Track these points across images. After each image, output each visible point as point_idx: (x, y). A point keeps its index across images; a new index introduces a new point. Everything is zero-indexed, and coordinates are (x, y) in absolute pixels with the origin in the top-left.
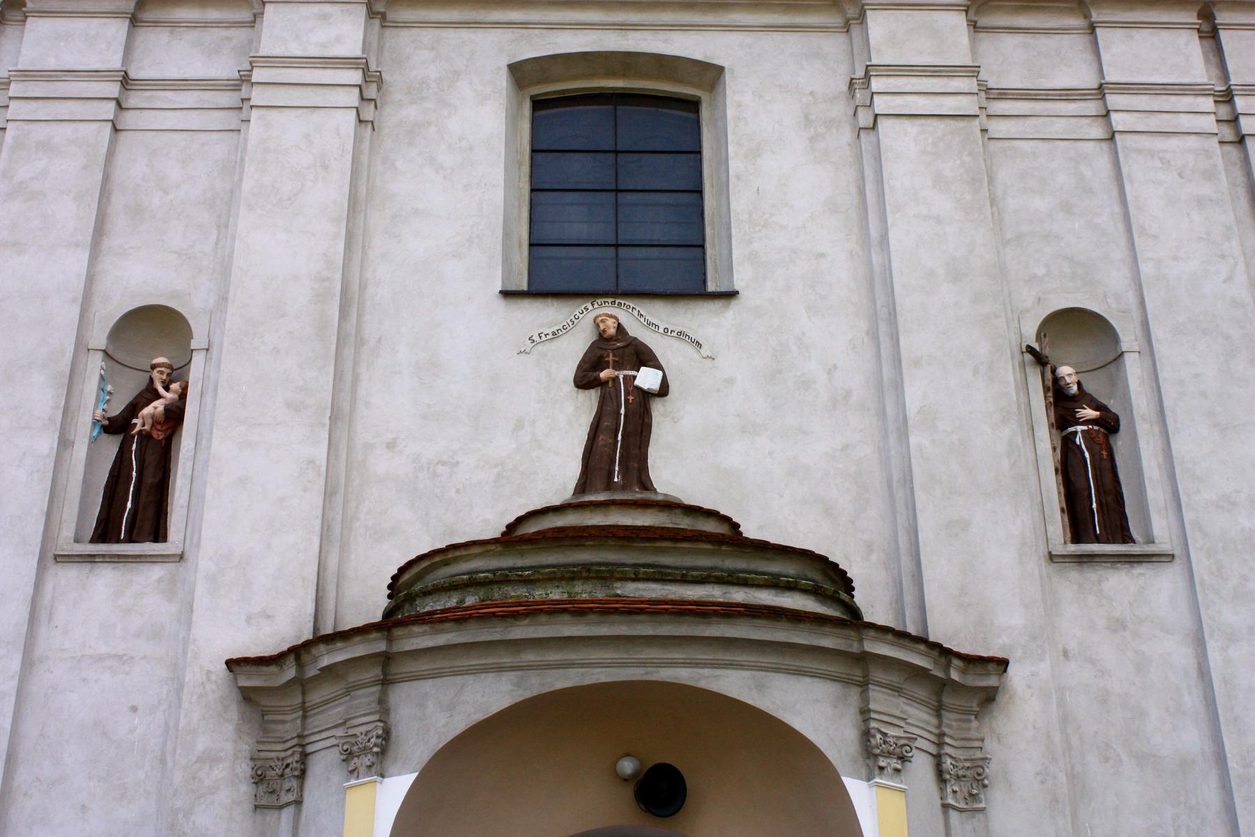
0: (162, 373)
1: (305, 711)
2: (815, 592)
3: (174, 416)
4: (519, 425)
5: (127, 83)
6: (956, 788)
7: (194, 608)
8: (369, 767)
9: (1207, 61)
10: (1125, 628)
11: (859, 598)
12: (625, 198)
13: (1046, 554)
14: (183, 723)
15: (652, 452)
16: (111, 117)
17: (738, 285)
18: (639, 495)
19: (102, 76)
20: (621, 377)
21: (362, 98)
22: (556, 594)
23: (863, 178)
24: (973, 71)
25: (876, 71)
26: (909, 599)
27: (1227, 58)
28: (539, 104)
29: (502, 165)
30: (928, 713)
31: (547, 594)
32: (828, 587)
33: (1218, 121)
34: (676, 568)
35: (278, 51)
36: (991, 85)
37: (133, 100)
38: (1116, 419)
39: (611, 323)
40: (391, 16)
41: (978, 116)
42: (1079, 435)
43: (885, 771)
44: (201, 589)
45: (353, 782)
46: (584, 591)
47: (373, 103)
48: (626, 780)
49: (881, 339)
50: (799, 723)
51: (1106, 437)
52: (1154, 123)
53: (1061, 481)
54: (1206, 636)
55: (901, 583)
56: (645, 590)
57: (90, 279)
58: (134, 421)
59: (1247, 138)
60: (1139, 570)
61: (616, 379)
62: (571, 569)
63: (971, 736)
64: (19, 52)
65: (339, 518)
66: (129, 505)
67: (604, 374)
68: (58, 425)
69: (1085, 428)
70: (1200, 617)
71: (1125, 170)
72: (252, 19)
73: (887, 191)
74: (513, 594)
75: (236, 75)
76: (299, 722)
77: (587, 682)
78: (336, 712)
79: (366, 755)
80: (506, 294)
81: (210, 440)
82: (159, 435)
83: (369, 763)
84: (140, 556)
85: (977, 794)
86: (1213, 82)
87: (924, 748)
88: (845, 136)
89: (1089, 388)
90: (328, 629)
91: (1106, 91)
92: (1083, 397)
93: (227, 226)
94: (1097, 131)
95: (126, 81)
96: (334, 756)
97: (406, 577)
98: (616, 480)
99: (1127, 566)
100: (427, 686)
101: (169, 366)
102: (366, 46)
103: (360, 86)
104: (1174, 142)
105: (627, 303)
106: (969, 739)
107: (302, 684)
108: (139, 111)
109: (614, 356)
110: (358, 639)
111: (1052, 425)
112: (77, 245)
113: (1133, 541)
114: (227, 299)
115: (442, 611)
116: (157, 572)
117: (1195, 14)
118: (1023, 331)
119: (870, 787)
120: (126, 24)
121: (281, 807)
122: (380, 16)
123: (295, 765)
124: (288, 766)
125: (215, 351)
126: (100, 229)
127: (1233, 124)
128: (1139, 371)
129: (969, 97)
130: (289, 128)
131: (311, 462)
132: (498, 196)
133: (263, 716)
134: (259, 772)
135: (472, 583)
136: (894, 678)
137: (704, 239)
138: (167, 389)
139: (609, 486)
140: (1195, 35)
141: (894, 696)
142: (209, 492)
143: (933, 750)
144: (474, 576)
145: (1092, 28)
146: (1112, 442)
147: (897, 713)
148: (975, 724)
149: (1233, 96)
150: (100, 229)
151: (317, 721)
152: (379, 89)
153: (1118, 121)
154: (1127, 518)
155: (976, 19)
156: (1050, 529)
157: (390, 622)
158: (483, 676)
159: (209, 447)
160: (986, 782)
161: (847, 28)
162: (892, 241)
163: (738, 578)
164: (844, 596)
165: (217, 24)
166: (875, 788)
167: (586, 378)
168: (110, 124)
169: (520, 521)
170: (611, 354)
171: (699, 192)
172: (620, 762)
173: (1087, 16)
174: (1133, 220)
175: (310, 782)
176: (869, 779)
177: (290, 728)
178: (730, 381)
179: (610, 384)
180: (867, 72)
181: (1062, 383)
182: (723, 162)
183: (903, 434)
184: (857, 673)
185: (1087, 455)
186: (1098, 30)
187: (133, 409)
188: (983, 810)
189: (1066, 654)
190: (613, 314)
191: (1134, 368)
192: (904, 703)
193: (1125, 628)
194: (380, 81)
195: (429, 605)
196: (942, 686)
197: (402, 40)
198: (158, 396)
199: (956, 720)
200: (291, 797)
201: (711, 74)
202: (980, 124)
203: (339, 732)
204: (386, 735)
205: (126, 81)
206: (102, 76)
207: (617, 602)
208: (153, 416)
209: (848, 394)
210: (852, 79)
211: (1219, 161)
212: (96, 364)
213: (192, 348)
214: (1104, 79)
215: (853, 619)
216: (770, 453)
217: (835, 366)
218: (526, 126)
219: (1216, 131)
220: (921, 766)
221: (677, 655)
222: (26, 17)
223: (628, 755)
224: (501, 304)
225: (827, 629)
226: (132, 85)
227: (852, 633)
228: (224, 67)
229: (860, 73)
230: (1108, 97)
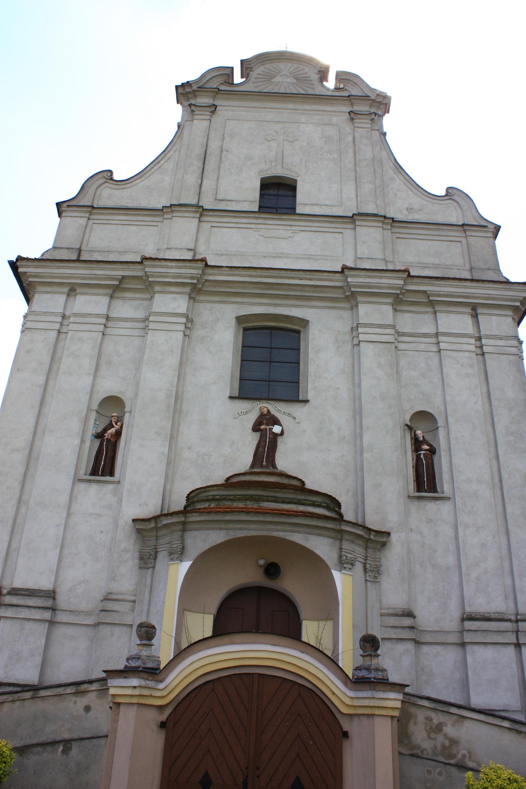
0: (115, 419)
1: (157, 538)
2: (327, 508)
3: (118, 434)
4: (233, 443)
5: (108, 319)
6: (370, 574)
7: (123, 501)
8: (177, 558)
9: (473, 325)
10: (432, 522)
11: (343, 510)
12: (272, 364)
13: (407, 495)
14: (117, 538)
15: (277, 455)
16: (102, 330)
17: (309, 398)
18: (271, 470)
19: (100, 316)
20: (268, 428)
21: (186, 327)
22: (241, 505)
23: (354, 362)
24: (393, 327)
25: (360, 325)
26: (360, 509)
27: (480, 325)
28: (245, 329)
29: (232, 352)
30: (362, 549)
31: (238, 505)
32: (332, 506)
33: (476, 347)
34: (281, 498)
35: (158, 310)
36: (400, 331)
37: (110, 324)
38: (435, 450)
39: (265, 410)
40: (197, 298)
41: (394, 343)
42: (422, 455)
43: (346, 569)
44: (125, 494)
45: (172, 562)
46: (250, 504)
47: (189, 329)
48: (261, 566)
49: (357, 419)
50: (318, 552)
51: (431, 455)
52: (454, 347)
53: (415, 471)
54: (459, 526)
55: (358, 504)
56: (270, 505)
57: (93, 386)
58: (105, 434)
59: (485, 354)
60: (438, 502)
61: (266, 429)
62: (246, 497)
63: (377, 557)
64: (74, 306)
65: (171, 472)
66: (102, 463)
67: (262, 427)
68: (81, 435)
69: (424, 452)
70: (457, 519)
71: (443, 363)
72: (150, 297)
73: (361, 367)
74: (227, 504)
75: (144, 317)
76: (155, 541)
77: (249, 535)
78: (167, 539)
79: (176, 554)
80: (231, 398)
81: (130, 443)
82: (113, 440)
83: (177, 557)
84: (106, 481)
85: (377, 577)
86: (475, 333)
87: (360, 561)
88: (349, 347)
89: (426, 438)
90: (165, 512)
91: (439, 335)
92: (425, 441)
93: (139, 369)
94: (435, 349)
95: (108, 318)
96: (165, 553)
97: (192, 495)
98: (264, 464)
99: (434, 501)
100: (197, 533)
101: (118, 417)
102: (188, 310)
103: (185, 324)
104: (461, 354)
105: (271, 403)
106: (376, 558)
107: (156, 529)
108: (111, 328)
109: (266, 421)
110: (175, 516)
111: (413, 451)
112: (89, 374)
113: (437, 492)
114: (137, 395)
115: (204, 509)
116: (111, 487)
117: (470, 309)
118: (405, 418)
119: (341, 573)
120: (109, 298)
121: (148, 568)
122: (193, 299)
123: (153, 555)
124: (151, 555)
125: (133, 412)
126: (97, 369)
127: (481, 348)
128: (443, 433)
129: (391, 336)
130: (161, 337)
131: (163, 453)
132: (230, 363)
133: (143, 538)
134: (142, 557)
135: (214, 500)
136: (351, 538)
137: (299, 380)
138: (116, 424)
139: (262, 466)
140: (470, 316)
141: (351, 544)
142: (129, 461)
143: (363, 561)
144: (214, 497)
145: (435, 312)
146: (433, 458)
147: (352, 549)
148: (378, 553)
149: (481, 339)
150: (97, 369)
151: (161, 541)
152: (192, 324)
153: (442, 346)
154: (436, 484)
155: (396, 307)
156: (410, 487)
157: (185, 512)
158: (215, 531)
159: (130, 446)
160: (380, 573)
161: (352, 308)
162: (362, 385)
163: (301, 502)
164: (337, 509)
165: (138, 299)
166: (342, 574)
167: (256, 428)
168: (102, 333)
169: (231, 477)
170: (265, 420)
171: (298, 363)
172: (260, 560)
173: (434, 308)
174: (445, 381)
175: (158, 561)
176: (340, 571)
177: (152, 543)
178: (305, 431)
179: (264, 430)
180: (357, 325)
181: (417, 436)
182: (307, 354)
183: (362, 453)
184: (339, 536)
185: (424, 462)
186: (437, 314)
187: (105, 430)
188: (379, 582)
189: (411, 530)
190: (267, 406)
191: (442, 432)
192: (354, 546)
193: (432, 522)
194: (192, 321)
195: (199, 506)
196: (368, 540)
197: (200, 307)
198: (113, 427)
199: (372, 552)
200: (152, 565)
201: (305, 323)
202: (395, 345)
203: (168, 545)
204: (183, 548)
205: (108, 318)
206: (100, 316)
207: (260, 509)
208: (111, 433)
209: (345, 437)
210: (352, 327)
211: (475, 361)
212: (94, 415)
213: (125, 411)
214: (438, 331)
215: (340, 518)
216: (317, 457)
217: (341, 427)
218: (241, 338)
219: (475, 351)
220: (359, 567)
221: (279, 527)
222: (77, 295)
223: (262, 558)
224: (228, 401)
225: (330, 521)
226: (110, 319)
227: (338, 523)
228: (140, 314)
229: (355, 325)
230: (439, 337)
